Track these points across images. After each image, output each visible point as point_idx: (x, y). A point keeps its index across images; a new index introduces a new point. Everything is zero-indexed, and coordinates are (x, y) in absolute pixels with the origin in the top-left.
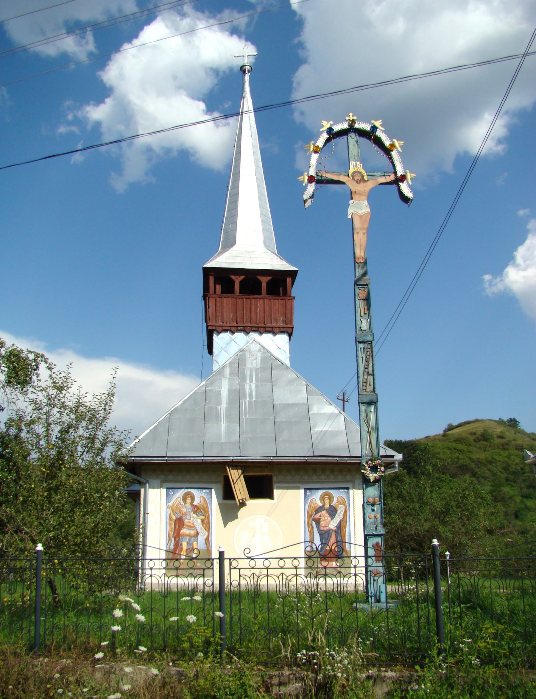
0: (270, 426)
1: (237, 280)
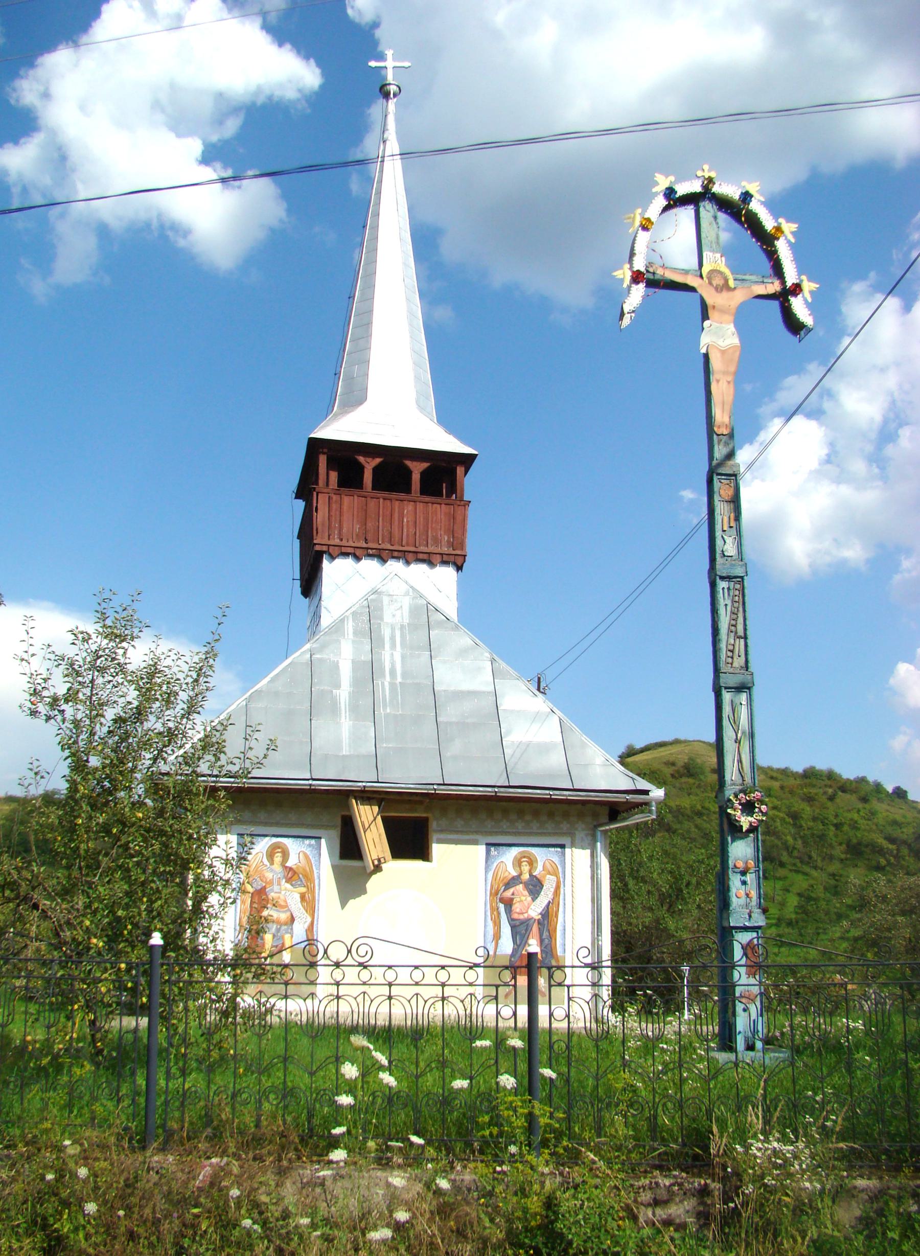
0: (429, 729)
1: (369, 465)
